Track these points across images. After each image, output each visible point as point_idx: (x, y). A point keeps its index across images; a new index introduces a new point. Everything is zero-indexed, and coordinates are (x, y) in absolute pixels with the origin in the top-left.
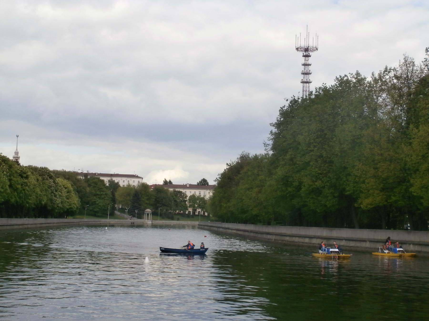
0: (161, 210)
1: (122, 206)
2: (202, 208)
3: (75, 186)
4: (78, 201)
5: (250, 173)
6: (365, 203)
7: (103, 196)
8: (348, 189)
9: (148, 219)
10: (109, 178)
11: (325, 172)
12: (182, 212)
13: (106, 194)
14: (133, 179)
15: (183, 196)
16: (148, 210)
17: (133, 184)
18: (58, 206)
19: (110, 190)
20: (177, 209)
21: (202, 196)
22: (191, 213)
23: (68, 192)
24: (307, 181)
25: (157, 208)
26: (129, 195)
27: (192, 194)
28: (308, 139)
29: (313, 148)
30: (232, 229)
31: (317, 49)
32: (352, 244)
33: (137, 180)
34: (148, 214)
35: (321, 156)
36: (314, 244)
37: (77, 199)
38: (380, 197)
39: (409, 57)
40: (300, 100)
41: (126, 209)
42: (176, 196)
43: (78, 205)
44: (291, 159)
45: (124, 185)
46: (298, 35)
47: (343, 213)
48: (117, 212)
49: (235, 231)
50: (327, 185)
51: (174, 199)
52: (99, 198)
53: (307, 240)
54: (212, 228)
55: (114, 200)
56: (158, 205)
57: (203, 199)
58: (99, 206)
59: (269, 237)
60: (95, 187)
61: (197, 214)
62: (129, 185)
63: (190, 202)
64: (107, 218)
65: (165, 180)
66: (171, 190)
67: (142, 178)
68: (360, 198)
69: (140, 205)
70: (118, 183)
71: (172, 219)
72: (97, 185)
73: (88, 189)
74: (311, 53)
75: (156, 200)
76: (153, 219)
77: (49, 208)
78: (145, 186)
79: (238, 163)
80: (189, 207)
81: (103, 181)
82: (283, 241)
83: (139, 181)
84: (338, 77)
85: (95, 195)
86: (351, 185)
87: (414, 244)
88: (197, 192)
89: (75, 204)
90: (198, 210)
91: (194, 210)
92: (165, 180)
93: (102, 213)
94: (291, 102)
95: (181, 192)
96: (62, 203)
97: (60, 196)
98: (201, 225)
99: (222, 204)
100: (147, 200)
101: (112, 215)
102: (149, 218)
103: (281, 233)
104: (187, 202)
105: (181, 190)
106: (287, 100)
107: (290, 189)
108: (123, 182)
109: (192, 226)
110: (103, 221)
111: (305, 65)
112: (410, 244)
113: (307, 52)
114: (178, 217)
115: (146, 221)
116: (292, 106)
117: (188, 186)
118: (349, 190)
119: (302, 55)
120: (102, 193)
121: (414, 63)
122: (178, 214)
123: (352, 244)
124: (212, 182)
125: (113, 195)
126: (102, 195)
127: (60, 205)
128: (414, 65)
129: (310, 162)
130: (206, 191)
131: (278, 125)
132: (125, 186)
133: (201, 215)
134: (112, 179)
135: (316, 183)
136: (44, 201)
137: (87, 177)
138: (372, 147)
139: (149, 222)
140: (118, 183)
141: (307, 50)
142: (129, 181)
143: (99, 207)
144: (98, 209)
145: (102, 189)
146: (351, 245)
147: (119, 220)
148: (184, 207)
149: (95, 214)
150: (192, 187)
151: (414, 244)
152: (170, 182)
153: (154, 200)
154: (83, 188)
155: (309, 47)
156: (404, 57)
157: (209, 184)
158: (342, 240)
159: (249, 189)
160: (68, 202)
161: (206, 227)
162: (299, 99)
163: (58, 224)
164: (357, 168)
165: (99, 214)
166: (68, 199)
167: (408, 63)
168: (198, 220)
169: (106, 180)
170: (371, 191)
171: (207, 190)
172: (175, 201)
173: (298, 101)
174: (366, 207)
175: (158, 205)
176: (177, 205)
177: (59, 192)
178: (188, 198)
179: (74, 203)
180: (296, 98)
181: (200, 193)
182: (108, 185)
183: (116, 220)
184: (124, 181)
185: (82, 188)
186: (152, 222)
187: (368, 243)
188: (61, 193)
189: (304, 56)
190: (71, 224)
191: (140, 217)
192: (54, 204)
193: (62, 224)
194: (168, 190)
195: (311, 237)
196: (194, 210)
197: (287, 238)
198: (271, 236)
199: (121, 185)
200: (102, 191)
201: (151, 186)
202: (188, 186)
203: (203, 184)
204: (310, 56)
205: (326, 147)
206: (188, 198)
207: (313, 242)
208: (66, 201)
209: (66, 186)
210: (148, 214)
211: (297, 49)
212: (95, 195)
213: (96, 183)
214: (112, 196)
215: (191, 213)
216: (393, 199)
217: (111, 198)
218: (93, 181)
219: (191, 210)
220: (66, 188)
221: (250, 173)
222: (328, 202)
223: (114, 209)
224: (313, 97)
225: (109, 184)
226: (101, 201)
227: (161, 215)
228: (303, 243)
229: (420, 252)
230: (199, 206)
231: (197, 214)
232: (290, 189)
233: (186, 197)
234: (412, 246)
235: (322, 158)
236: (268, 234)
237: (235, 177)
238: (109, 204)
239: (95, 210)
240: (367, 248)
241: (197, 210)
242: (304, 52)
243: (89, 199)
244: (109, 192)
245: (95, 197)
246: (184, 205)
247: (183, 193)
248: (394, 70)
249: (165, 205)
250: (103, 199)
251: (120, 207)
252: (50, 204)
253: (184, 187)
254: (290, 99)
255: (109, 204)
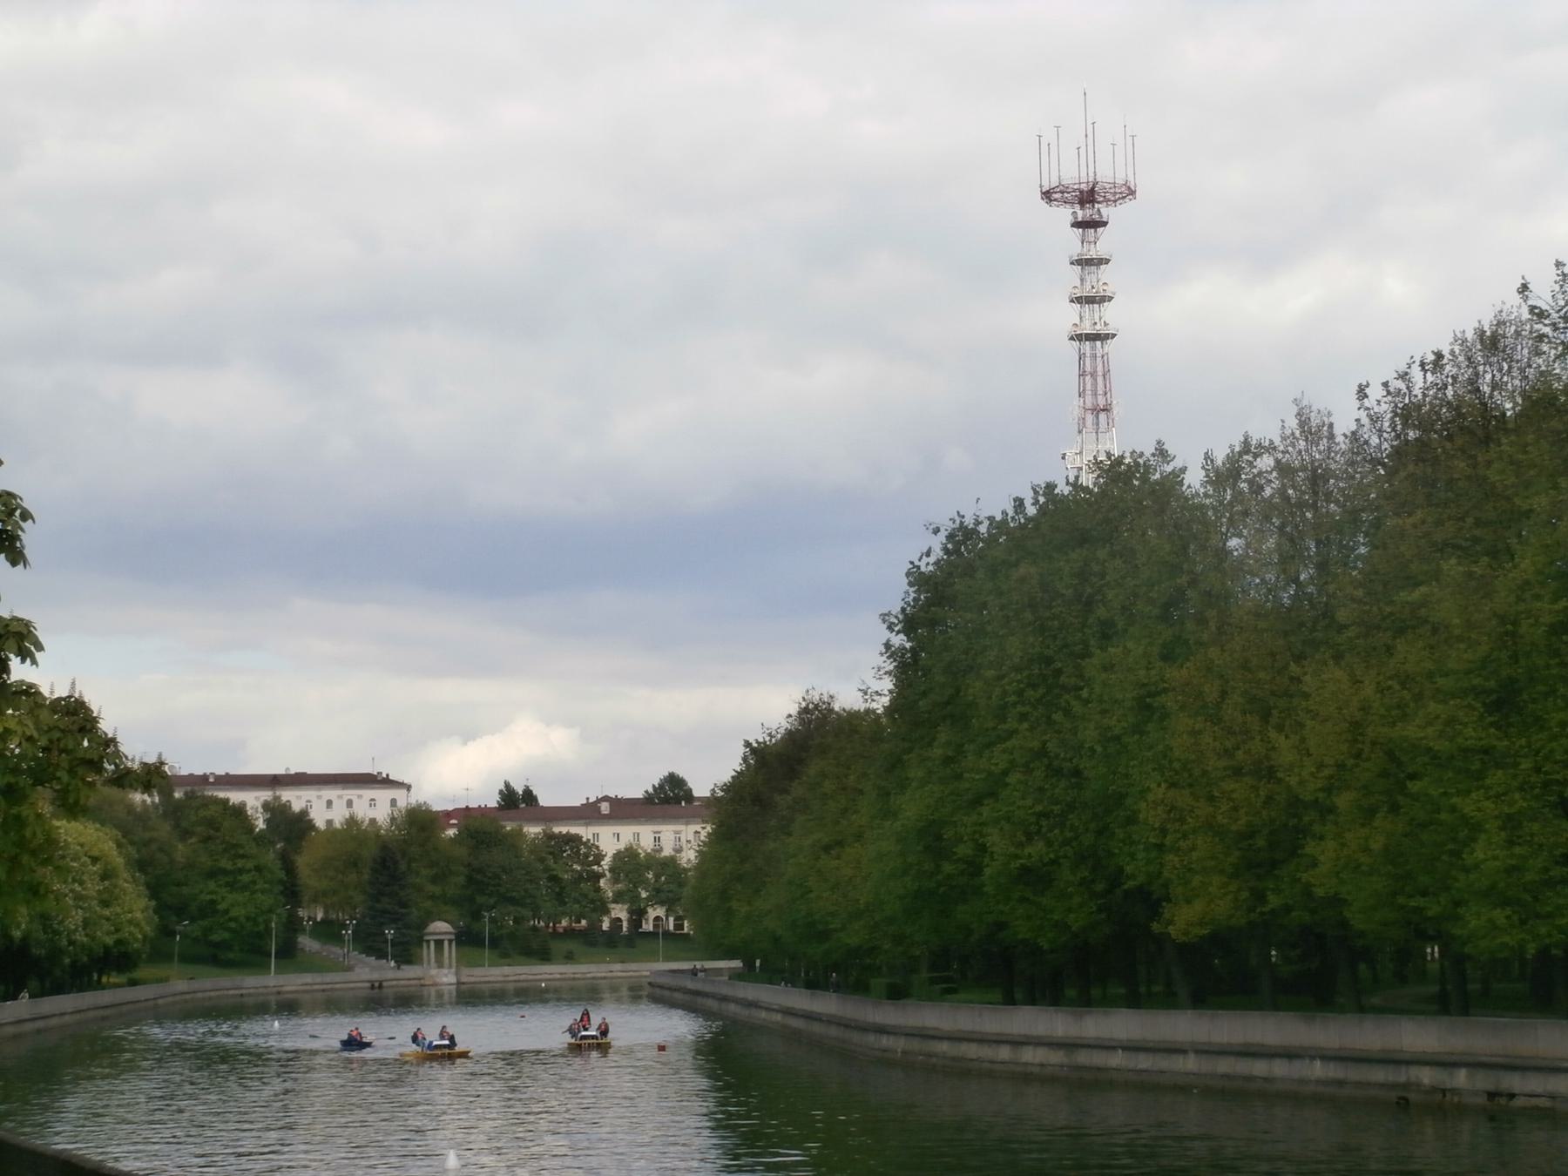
0: (493, 920)
1: (326, 912)
2: (670, 903)
3: (130, 848)
4: (147, 908)
5: (828, 786)
6: (1183, 920)
7: (246, 878)
8: (1129, 869)
9: (440, 965)
10: (266, 795)
11: (1056, 808)
12: (584, 922)
13: (258, 869)
14: (368, 793)
15: (587, 856)
16: (440, 927)
17: (371, 814)
18: (71, 943)
19: (273, 843)
20: (564, 914)
21: (667, 852)
22: (625, 924)
23: (105, 876)
24: (997, 841)
25: (476, 916)
26: (353, 863)
27: (621, 846)
28: (998, 691)
29: (1015, 725)
30: (768, 1009)
31: (1132, 193)
32: (1144, 1062)
33: (383, 795)
34: (439, 943)
35: (1042, 752)
36: (1026, 1064)
37: (143, 902)
38: (1230, 897)
39: (1314, 408)
40: (983, 529)
41: (345, 927)
42: (556, 855)
43: (147, 928)
44: (947, 761)
45: (329, 822)
46: (1049, 136)
47: (1116, 957)
48: (306, 942)
49: (778, 1017)
50: (1066, 857)
51: (547, 869)
52: (227, 884)
53: (1004, 1053)
54: (700, 1000)
55: (292, 893)
56: (480, 899)
57: (671, 862)
58: (231, 920)
59: (886, 1041)
60: (209, 838)
61: (648, 926)
62: (352, 822)
63: (616, 880)
64: (263, 967)
65: (507, 785)
66: (533, 830)
67: (409, 788)
68: (1169, 900)
69: (404, 905)
70: (304, 813)
71: (544, 956)
72: (218, 830)
73: (181, 851)
74: (1107, 211)
75: (470, 879)
76: (463, 961)
77: (38, 951)
78: (421, 821)
79: (790, 734)
80: (615, 901)
81: (239, 811)
82: (930, 1055)
83: (393, 802)
84: (1102, 457)
85: (212, 874)
86: (1140, 855)
87: (1327, 1057)
88: (644, 836)
89: (137, 925)
90: (652, 913)
91: (638, 915)
92: (507, 785)
93: (248, 948)
94: (950, 537)
95: (574, 840)
96: (86, 923)
97: (79, 897)
98: (661, 987)
99: (734, 904)
100: (434, 880)
101: (288, 953)
102: (446, 961)
103: (924, 1028)
104: (602, 882)
105: (574, 830)
106: (936, 531)
107: (948, 868)
108: (325, 810)
109: (631, 989)
110: (253, 983)
111: (1084, 263)
112: (1313, 1058)
113: (1088, 204)
114: (570, 945)
115: (434, 972)
116: (957, 551)
117: (605, 808)
118: (1136, 870)
119: (1070, 219)
120: (240, 863)
121: (1331, 426)
122: (570, 933)
123: (1144, 1062)
124: (701, 788)
125: (289, 868)
126: (241, 871)
127: (80, 937)
128: (1331, 436)
129: (1005, 773)
130: (681, 827)
131: (910, 623)
132: (337, 825)
133: (667, 934)
134: (277, 798)
135: (1028, 850)
136: (18, 926)
137: (170, 794)
138: (1197, 727)
139: (446, 978)
140: (304, 813)
141: (1088, 197)
142: (350, 804)
143: (233, 925)
144: (226, 935)
145: (242, 847)
146: (1140, 1066)
147: (318, 978)
148: (592, 902)
149: (214, 956)
150: (623, 810)
151: (1327, 1057)
152: (529, 797)
153: (461, 880)
154: (161, 850)
155: (1095, 183)
156: (1295, 410)
157: (696, 794)
158: (1114, 1048)
159: (827, 849)
160: (108, 919)
161: (678, 996)
162: (978, 523)
163: (78, 1017)
164: (1151, 797)
165: (231, 956)
166: (105, 904)
167: (1311, 429)
168: (653, 956)
169: (253, 800)
170: (1196, 881)
171: (687, 824)
172: (554, 879)
173: (975, 531)
174: (1186, 933)
175: (480, 899)
176: (560, 898)
177: (74, 880)
178: (606, 863)
179: (130, 922)
180: (969, 521)
181: (657, 840)
182: (261, 824)
183: (308, 978)
184: (329, 803)
185: (154, 847)
186: (457, 974)
187: (1192, 1056)
188: (81, 883)
189: (1077, 224)
190: (124, 1008)
191: (406, 954)
192: (56, 932)
193: (91, 1014)
194: (519, 833)
195: (1017, 1043)
196: (638, 915)
197: (944, 1047)
198: (892, 1038)
199: (320, 824)
200: (243, 856)
201: (448, 815)
202: (605, 808)
203: (670, 797)
204: (1105, 224)
205: (1058, 717)
206: (606, 863)
207: (1024, 1060)
208: (101, 917)
209: (95, 853)
210: (439, 943)
211: (1047, 195)
212: (212, 874)
213: (212, 824)
214: (282, 875)
215: (625, 924)
216: (1274, 901)
217: (280, 882)
218: (202, 813)
219: (620, 912)
220: (95, 860)
221: (828, 786)
222: (1072, 916)
223: (293, 926)
224: (1031, 511)
225: (267, 821)
226: (239, 897)
227: (495, 943)
228: (992, 1062)
229: (1340, 1083)
230: (658, 897)
231: (648, 926)
232: (948, 868)
233: (599, 858)
234: (1318, 1063)
235: (1045, 761)
236: (881, 1030)
237: (777, 798)
238: (270, 911)
239: (215, 937)
240: (1187, 1074)
241: (650, 910)
242: (1077, 208)
243: (185, 890)
244: (270, 857)
245: (212, 885)
246: (592, 895)
247: (585, 844)
248: (1272, 448)
249: (513, 901)
250: (245, 888)
251: (320, 916)
252: (43, 937)
253: (589, 813)
254: (947, 526)
255: (270, 911)
